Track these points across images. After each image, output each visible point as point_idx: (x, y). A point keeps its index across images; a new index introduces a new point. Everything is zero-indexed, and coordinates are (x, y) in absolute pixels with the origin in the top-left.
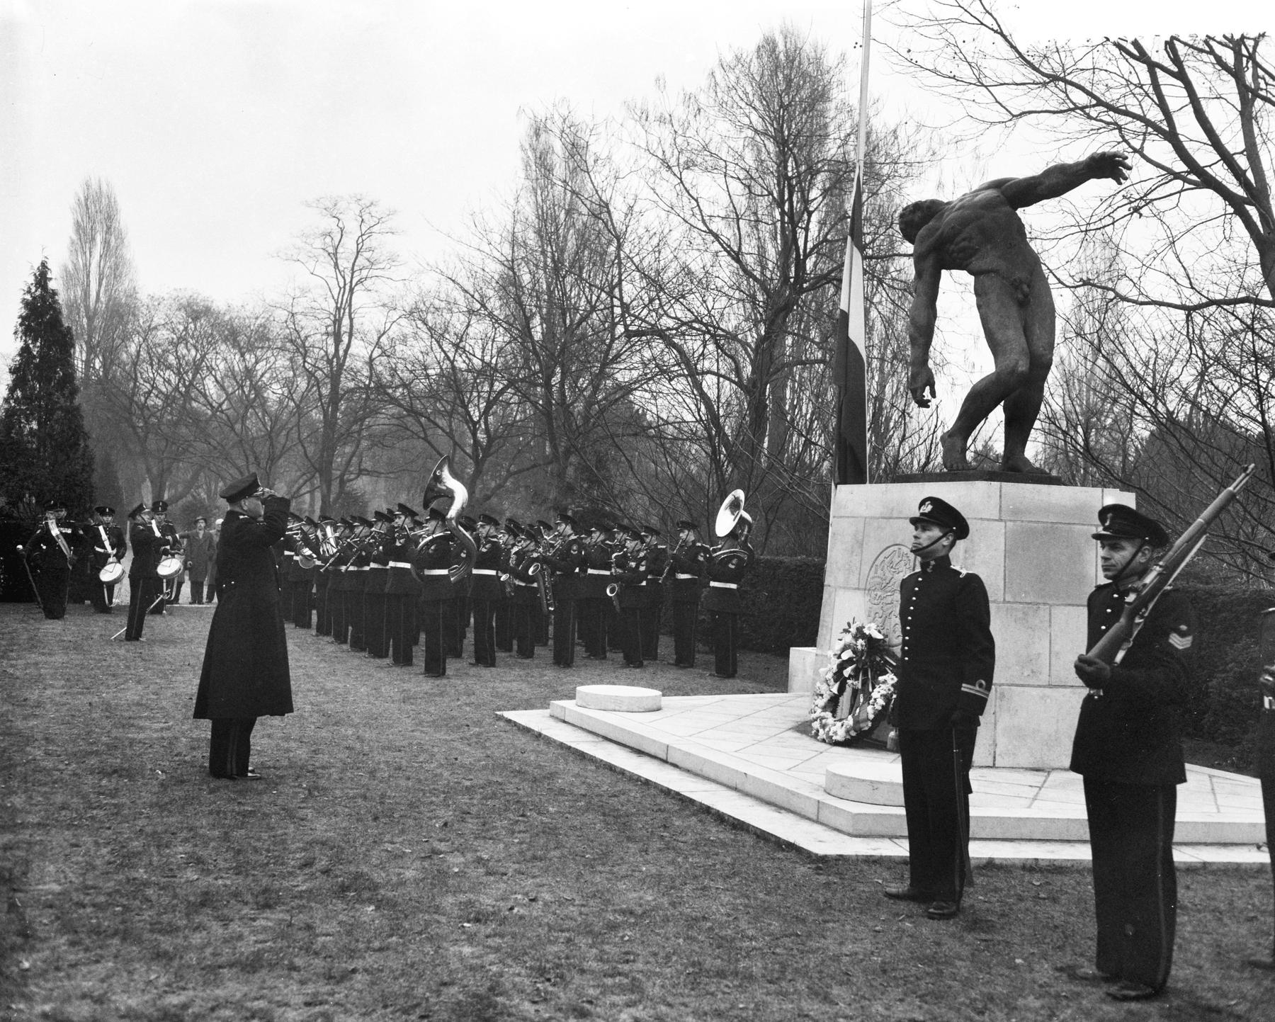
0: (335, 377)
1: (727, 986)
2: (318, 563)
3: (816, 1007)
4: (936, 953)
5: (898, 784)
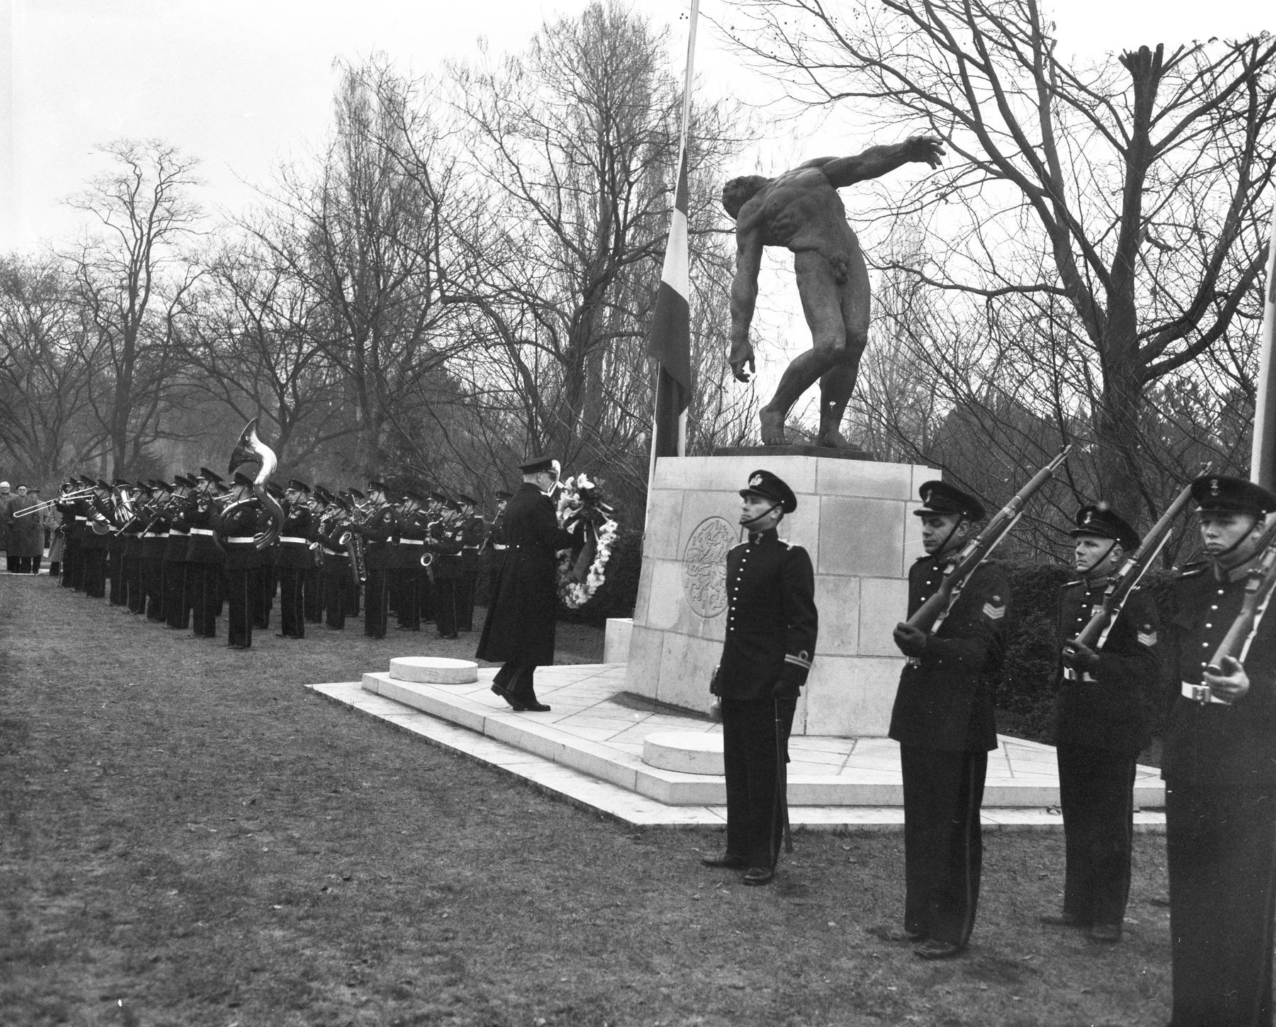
0: (130, 334)
1: (548, 960)
2: (112, 528)
3: (638, 978)
4: (752, 919)
5: (719, 754)
